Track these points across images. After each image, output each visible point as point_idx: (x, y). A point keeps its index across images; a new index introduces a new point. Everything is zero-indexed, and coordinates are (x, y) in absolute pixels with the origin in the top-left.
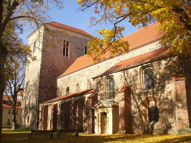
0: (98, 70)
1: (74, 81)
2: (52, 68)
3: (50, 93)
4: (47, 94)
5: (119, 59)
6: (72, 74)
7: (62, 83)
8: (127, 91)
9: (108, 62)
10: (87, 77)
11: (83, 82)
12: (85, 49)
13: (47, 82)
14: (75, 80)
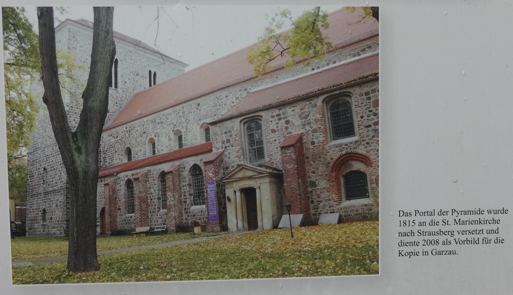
0: (196, 111)
1: (141, 136)
6: (137, 121)
7: (113, 140)
9: (220, 96)
10: (172, 126)
11: (164, 135)
14: (144, 133)
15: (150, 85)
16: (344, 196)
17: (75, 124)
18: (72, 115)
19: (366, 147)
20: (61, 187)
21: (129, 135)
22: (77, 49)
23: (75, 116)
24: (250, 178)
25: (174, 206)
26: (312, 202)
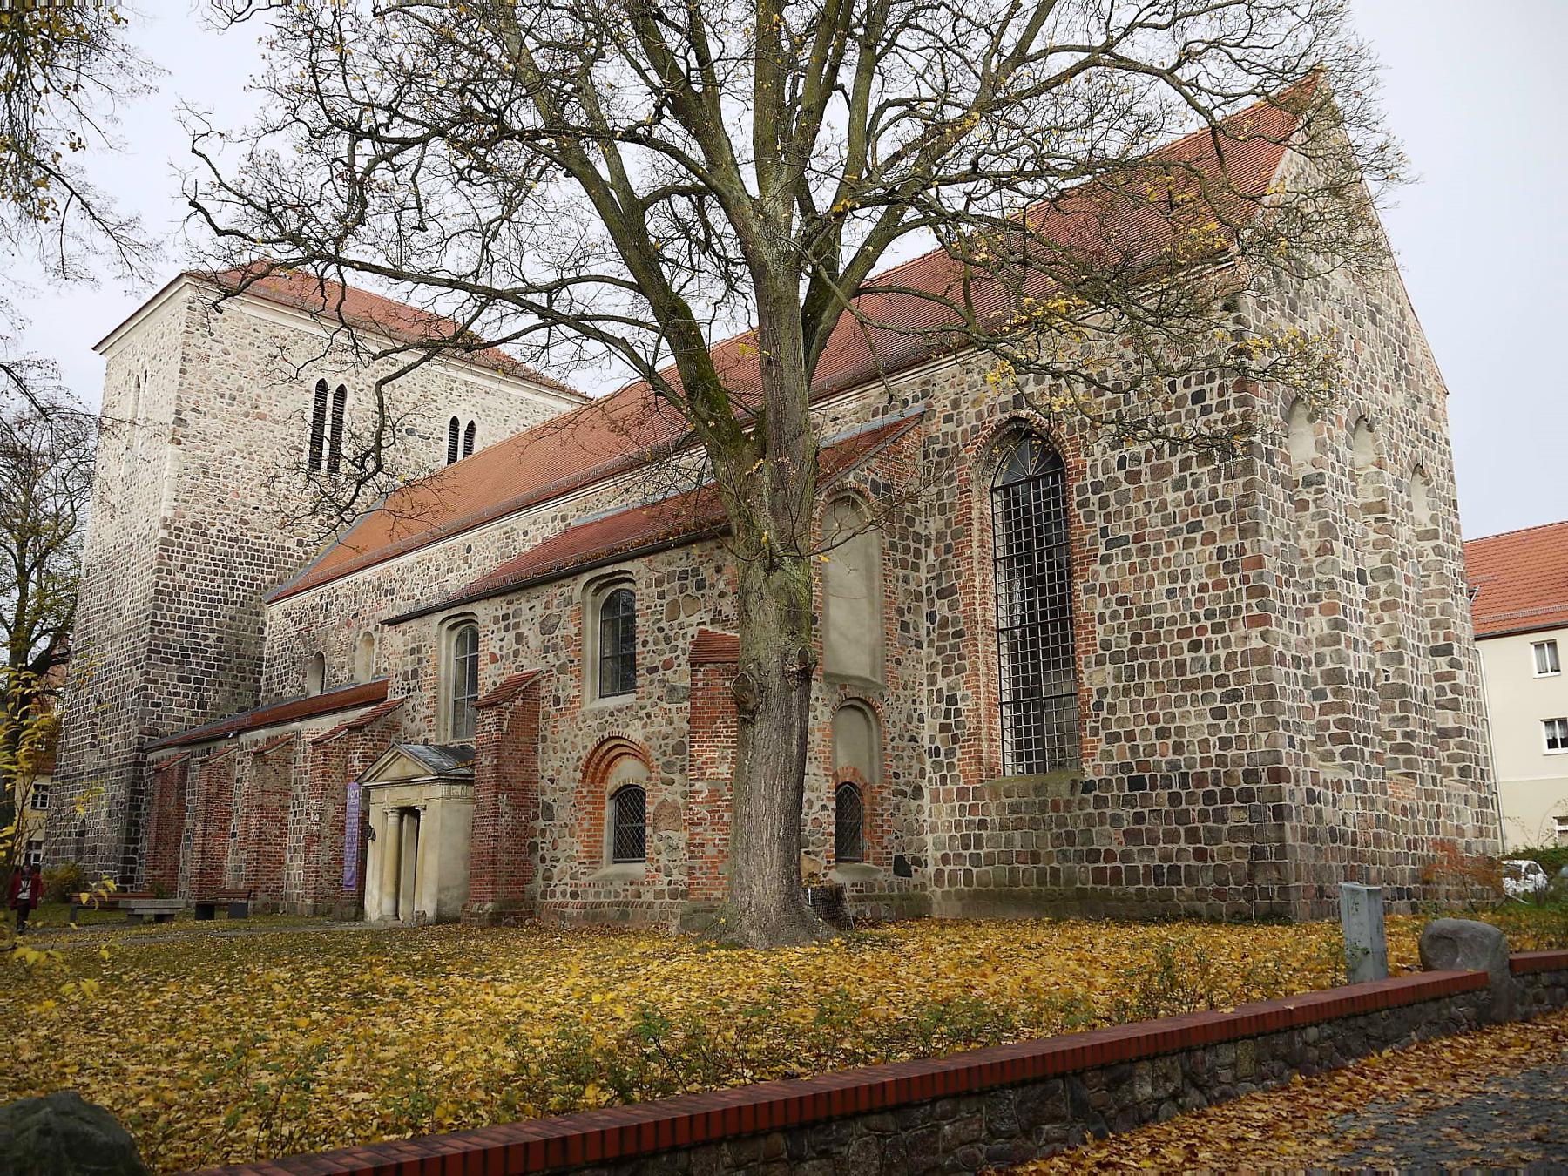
2: (236, 540)
3: (221, 684)
4: (198, 689)
5: (564, 519)
8: (519, 702)
9: (513, 530)
12: (446, 436)
13: (199, 621)
15: (452, 458)
16: (607, 851)
17: (184, 578)
18: (178, 552)
19: (645, 726)
20: (125, 759)
21: (325, 618)
22: (213, 361)
23: (186, 557)
24: (407, 781)
25: (319, 837)
26: (543, 860)
